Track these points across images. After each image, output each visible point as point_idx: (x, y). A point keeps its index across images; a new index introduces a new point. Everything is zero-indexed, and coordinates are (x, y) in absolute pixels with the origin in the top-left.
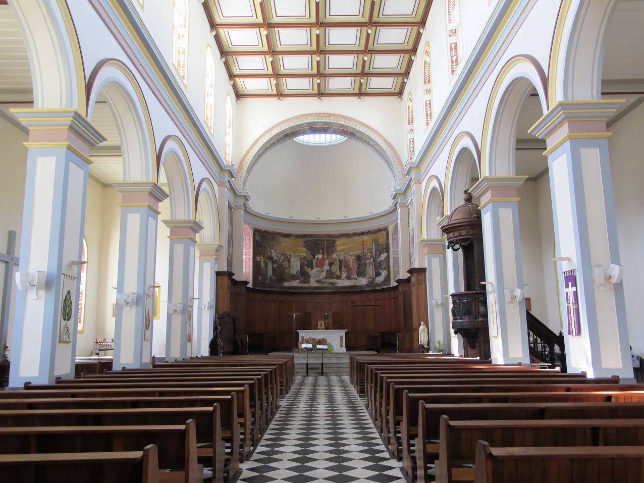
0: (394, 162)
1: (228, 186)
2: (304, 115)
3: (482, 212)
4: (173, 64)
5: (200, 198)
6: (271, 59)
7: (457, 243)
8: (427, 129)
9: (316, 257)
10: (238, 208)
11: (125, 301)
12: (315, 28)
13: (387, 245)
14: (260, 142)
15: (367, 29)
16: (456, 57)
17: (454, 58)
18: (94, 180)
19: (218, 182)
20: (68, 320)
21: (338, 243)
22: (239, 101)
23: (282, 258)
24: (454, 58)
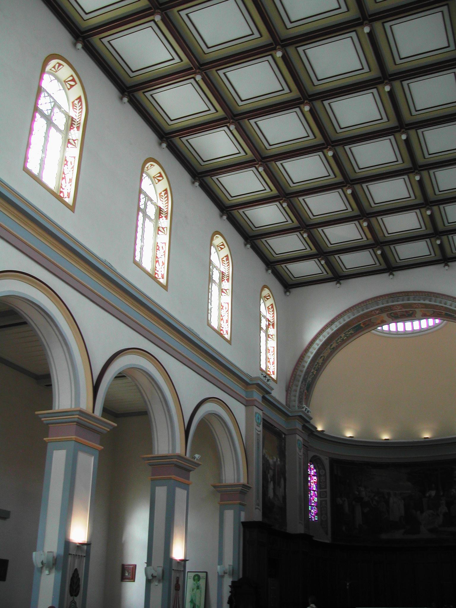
0: (296, 391)
9: (427, 495)
10: (293, 432)
11: (152, 574)
14: (318, 341)
18: (215, 331)
19: (244, 403)
20: (76, 596)
22: (288, 293)
23: (376, 498)
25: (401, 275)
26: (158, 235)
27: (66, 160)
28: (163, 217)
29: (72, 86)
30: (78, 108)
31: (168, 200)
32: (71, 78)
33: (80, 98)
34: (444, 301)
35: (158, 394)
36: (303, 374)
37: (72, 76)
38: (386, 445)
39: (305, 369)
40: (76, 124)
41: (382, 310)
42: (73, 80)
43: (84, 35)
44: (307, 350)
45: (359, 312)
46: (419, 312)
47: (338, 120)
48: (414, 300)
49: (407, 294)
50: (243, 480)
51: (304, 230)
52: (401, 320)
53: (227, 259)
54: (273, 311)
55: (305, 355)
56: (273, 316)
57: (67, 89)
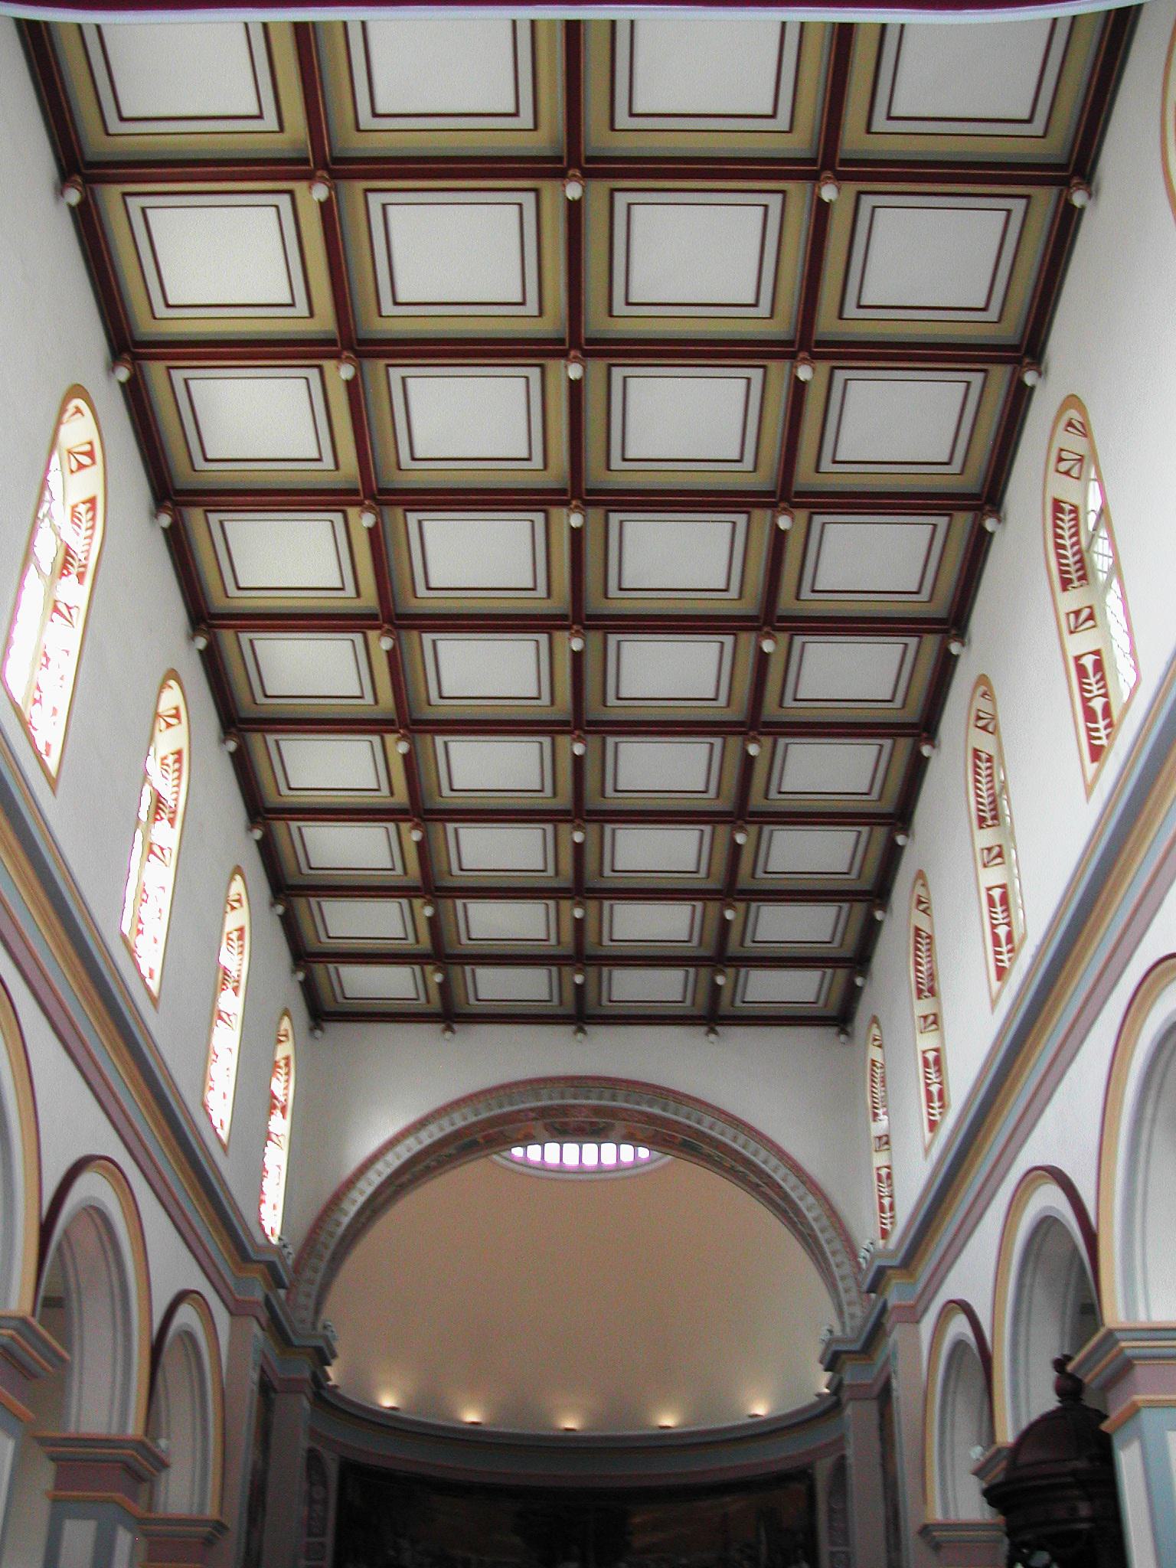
1: (264, 1315)
2: (531, 1082)
3: (1116, 1442)
4: (123, 936)
5: (166, 1359)
6: (403, 748)
7: (1042, 1548)
8: (931, 1143)
12: (567, 634)
13: (811, 1532)
14: (380, 1166)
15: (758, 637)
16: (1103, 700)
17: (1002, 931)
19: (228, 1298)
21: (637, 1520)
22: (318, 1033)
24: (1002, 931)
25: (602, 1036)
26: (147, 863)
27: (45, 654)
28: (162, 818)
29: (81, 466)
30: (84, 525)
31: (179, 778)
32: (87, 448)
33: (92, 501)
34: (696, 1114)
35: (109, 1276)
36: (333, 1243)
37: (91, 443)
38: (471, 1439)
39: (340, 1230)
40: (76, 564)
41: (543, 1112)
42: (90, 454)
43: (140, 350)
44: (351, 1183)
45: (491, 1110)
46: (620, 1127)
47: (621, 671)
48: (627, 1101)
49: (612, 1084)
50: (211, 1511)
51: (428, 897)
52: (574, 1139)
53: (241, 938)
54: (287, 1074)
55: (344, 1194)
56: (286, 1088)
57: (67, 472)
